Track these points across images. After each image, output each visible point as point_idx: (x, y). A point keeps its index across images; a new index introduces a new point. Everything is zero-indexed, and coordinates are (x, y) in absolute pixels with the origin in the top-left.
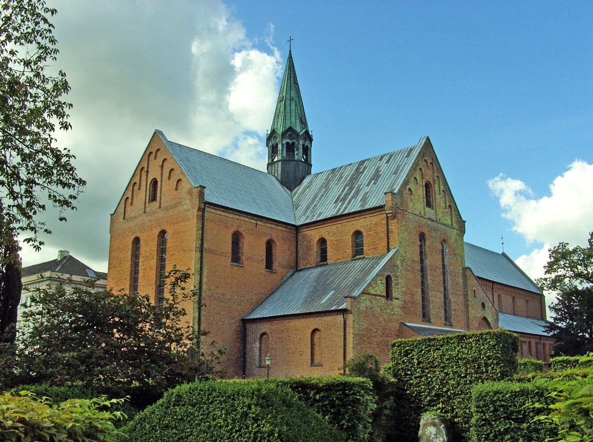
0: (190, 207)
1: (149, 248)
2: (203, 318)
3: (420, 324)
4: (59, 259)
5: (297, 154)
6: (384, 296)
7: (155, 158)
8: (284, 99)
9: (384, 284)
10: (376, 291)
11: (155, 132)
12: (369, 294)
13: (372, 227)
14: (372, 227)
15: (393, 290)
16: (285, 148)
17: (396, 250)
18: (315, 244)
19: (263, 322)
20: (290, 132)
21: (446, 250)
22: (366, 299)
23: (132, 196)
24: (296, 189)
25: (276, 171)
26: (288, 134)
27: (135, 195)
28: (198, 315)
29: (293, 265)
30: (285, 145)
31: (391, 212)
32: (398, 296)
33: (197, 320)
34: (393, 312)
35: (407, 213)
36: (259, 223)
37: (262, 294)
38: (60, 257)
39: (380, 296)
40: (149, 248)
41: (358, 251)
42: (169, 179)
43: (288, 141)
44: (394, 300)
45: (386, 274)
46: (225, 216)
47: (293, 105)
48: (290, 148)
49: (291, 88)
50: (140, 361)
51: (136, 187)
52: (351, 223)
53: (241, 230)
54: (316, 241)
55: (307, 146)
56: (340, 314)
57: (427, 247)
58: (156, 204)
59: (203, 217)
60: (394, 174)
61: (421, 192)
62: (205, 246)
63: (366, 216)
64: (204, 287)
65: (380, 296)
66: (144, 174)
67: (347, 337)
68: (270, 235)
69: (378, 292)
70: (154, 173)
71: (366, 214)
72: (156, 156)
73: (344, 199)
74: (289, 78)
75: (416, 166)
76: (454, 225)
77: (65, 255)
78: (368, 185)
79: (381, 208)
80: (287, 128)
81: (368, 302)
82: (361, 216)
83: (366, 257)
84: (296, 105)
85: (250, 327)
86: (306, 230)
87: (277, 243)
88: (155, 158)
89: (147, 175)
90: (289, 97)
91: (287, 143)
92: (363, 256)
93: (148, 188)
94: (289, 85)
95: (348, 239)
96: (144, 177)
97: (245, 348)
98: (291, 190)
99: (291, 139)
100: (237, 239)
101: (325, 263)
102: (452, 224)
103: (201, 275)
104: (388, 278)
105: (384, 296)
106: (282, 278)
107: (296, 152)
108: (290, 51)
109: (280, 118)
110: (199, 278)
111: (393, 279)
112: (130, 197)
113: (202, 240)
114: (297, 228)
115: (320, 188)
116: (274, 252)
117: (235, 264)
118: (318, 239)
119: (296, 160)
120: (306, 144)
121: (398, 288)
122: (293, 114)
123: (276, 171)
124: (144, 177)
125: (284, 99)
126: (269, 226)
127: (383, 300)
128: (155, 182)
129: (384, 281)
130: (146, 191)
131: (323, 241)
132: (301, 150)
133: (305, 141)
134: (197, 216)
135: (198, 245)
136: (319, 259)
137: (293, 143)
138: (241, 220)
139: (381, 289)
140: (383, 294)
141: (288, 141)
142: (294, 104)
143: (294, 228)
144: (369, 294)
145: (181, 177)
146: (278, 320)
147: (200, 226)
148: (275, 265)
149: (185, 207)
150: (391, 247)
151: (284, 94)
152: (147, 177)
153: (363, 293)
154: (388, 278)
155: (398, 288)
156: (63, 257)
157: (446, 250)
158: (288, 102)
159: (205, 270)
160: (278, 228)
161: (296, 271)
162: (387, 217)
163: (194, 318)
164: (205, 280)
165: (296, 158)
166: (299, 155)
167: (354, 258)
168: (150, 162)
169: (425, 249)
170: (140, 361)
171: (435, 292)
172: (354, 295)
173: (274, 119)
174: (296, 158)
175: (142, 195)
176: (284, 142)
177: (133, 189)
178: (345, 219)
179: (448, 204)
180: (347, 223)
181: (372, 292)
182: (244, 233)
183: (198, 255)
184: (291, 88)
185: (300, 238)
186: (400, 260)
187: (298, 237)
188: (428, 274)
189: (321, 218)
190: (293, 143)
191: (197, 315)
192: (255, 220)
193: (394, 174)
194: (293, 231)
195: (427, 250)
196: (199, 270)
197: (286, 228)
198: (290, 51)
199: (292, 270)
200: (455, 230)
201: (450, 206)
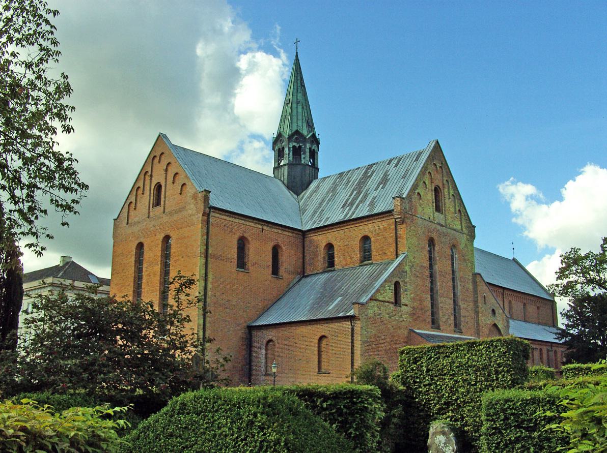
0: (195, 213)
1: (153, 254)
2: (208, 325)
4: (61, 265)
5: (304, 158)
6: (392, 303)
7: (159, 162)
8: (291, 102)
9: (392, 290)
11: (159, 136)
12: (377, 300)
15: (402, 296)
16: (291, 152)
17: (404, 255)
20: (296, 135)
22: (374, 306)
23: (136, 200)
25: (282, 175)
26: (294, 137)
27: (138, 200)
28: (202, 322)
29: (299, 270)
30: (292, 149)
33: (202, 326)
34: (402, 319)
36: (265, 228)
38: (62, 262)
39: (388, 302)
40: (153, 254)
42: (173, 183)
43: (295, 144)
44: (403, 307)
45: (395, 280)
46: (230, 221)
49: (297, 91)
51: (140, 192)
52: (359, 228)
53: (246, 235)
54: (323, 247)
55: (314, 150)
57: (436, 253)
58: (160, 209)
59: (208, 222)
62: (210, 251)
64: (209, 293)
65: (388, 302)
66: (148, 178)
67: (355, 342)
68: (276, 240)
70: (158, 177)
71: (375, 219)
75: (425, 170)
76: (464, 230)
77: (68, 260)
78: (376, 189)
81: (376, 309)
82: (368, 221)
83: (374, 262)
84: (303, 108)
87: (284, 248)
88: (159, 162)
91: (294, 147)
94: (295, 87)
95: (356, 244)
96: (148, 182)
97: (250, 355)
99: (298, 143)
100: (242, 244)
101: (333, 269)
102: (462, 230)
103: (206, 280)
104: (397, 284)
105: (392, 303)
106: (289, 284)
108: (297, 53)
109: (286, 122)
110: (203, 284)
111: (402, 285)
112: (134, 202)
114: (304, 234)
118: (325, 244)
120: (313, 148)
123: (282, 175)
124: (148, 182)
125: (291, 102)
126: (276, 231)
127: (392, 306)
128: (159, 187)
129: (393, 287)
131: (330, 247)
132: (308, 154)
135: (203, 251)
136: (327, 265)
139: (389, 295)
140: (391, 300)
141: (295, 144)
142: (301, 107)
146: (285, 327)
147: (205, 231)
148: (282, 271)
149: (190, 212)
150: (400, 252)
151: (291, 97)
153: (371, 299)
154: (397, 284)
155: (407, 294)
156: (65, 262)
158: (294, 105)
160: (284, 233)
164: (210, 286)
165: (303, 162)
166: (305, 159)
168: (154, 166)
169: (434, 254)
172: (361, 301)
173: (281, 122)
174: (303, 162)
175: (146, 200)
176: (291, 146)
178: (353, 224)
179: (457, 209)
180: (355, 228)
181: (381, 298)
182: (250, 239)
183: (203, 260)
185: (307, 243)
189: (328, 223)
190: (300, 147)
191: (201, 322)
192: (261, 225)
194: (300, 236)
196: (204, 276)
198: (297, 53)
201: (459, 210)
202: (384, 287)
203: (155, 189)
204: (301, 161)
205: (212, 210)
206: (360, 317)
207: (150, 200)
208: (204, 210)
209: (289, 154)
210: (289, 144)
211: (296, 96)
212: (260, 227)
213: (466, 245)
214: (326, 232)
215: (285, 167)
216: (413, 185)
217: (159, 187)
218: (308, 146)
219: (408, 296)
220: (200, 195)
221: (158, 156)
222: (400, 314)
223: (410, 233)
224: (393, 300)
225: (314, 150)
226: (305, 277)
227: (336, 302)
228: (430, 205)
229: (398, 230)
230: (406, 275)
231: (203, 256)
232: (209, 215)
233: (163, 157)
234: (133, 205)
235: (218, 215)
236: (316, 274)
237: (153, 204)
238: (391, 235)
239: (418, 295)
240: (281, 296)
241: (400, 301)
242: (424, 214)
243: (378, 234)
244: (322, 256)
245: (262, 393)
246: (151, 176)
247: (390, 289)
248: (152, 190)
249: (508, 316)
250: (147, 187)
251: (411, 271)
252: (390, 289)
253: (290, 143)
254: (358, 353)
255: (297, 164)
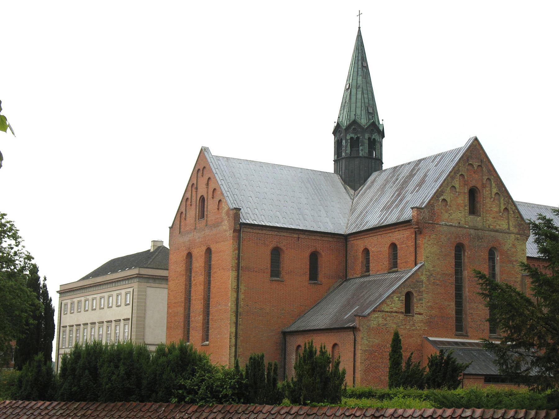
0: (226, 227)
1: (198, 264)
2: (240, 332)
3: (451, 338)
4: (152, 250)
5: (362, 150)
6: (402, 313)
7: (202, 176)
8: (350, 88)
9: (403, 300)
10: (392, 309)
11: (202, 149)
12: (383, 311)
13: (404, 241)
14: (404, 241)
15: (415, 305)
16: (349, 144)
17: (421, 264)
18: (360, 254)
19: (298, 335)
20: (354, 125)
21: (498, 258)
22: (377, 317)
23: (186, 211)
24: (360, 188)
25: (341, 169)
26: (352, 128)
27: (187, 211)
28: (235, 330)
29: (341, 274)
30: (349, 141)
31: (417, 227)
32: (422, 312)
33: (234, 334)
34: (415, 328)
35: (438, 226)
36: (301, 236)
37: (306, 306)
38: (152, 247)
39: (396, 312)
40: (198, 264)
41: (394, 265)
42: (213, 198)
43: (353, 135)
44: (416, 316)
45: (406, 290)
46: (263, 234)
47: (360, 94)
48: (355, 143)
49: (358, 74)
50: (529, 340)
51: (189, 203)
52: (388, 235)
53: (280, 245)
54: (361, 251)
55: (374, 139)
56: (350, 331)
57: (466, 258)
58: (203, 222)
59: (239, 237)
60: (434, 182)
61: (463, 200)
62: (242, 264)
63: (400, 229)
64: (241, 303)
65: (396, 312)
66: (194, 190)
67: (357, 352)
68: (314, 246)
69: (394, 309)
70: (202, 191)
71: (400, 227)
72: (203, 173)
73: (389, 207)
74: (356, 61)
75: (455, 173)
76: (511, 229)
77: (159, 245)
78: (412, 193)
79: (407, 223)
80: (351, 121)
81: (380, 319)
82: (395, 228)
83: (399, 270)
84: (363, 93)
85: (290, 340)
86: (353, 239)
87: (323, 254)
88: (202, 176)
89: (197, 194)
90: (355, 84)
91: (352, 138)
92: (397, 269)
93: (198, 204)
94: (356, 70)
95: (385, 249)
96: (194, 193)
97: (285, 358)
98: (355, 189)
99: (356, 134)
100: (276, 253)
101: (367, 274)
102: (509, 228)
103: (238, 292)
104: (409, 296)
105: (402, 313)
106: (329, 289)
107: (361, 148)
108: (359, 28)
109: (346, 110)
110: (236, 296)
111: (415, 295)
112: (184, 212)
113: (238, 259)
114: (344, 239)
115: (378, 190)
116: (319, 262)
117: (274, 279)
118: (362, 249)
119: (360, 157)
120: (373, 137)
121: (422, 303)
122: (359, 104)
123: (341, 169)
124: (194, 193)
125: (350, 88)
126: (313, 238)
127: (401, 316)
128: (203, 199)
129: (403, 298)
130: (196, 208)
131: (366, 251)
132: (367, 145)
133: (372, 134)
134: (233, 236)
135: (234, 265)
136: (365, 269)
137: (358, 138)
138: (281, 236)
139: (398, 304)
140: (401, 311)
141: (353, 135)
142: (361, 92)
143: (342, 237)
144: (383, 311)
145: (221, 197)
146: (309, 334)
147: (237, 246)
148: (321, 276)
149: (224, 227)
150: (418, 261)
151: (351, 81)
152: (197, 194)
153: (374, 311)
154: (409, 296)
155: (422, 303)
156: (156, 248)
157: (498, 258)
158: (354, 91)
159: (242, 287)
160: (324, 239)
161: (345, 281)
162: (415, 231)
163: (231, 333)
164: (242, 296)
165: (361, 155)
166: (363, 151)
167: (391, 271)
168: (199, 178)
169: (464, 259)
170: (529, 340)
171: (476, 304)
172: (364, 314)
173: (341, 110)
174: (361, 155)
175: (192, 213)
176: (348, 137)
177: (186, 204)
178: (383, 231)
179: (503, 207)
180: (385, 235)
181: (387, 309)
182: (284, 248)
183: (234, 274)
184: (358, 74)
185: (349, 247)
186: (426, 275)
187: (348, 246)
188: (467, 285)
189: (365, 228)
190: (358, 138)
191: (233, 330)
192: (297, 234)
193: (434, 182)
194: (341, 240)
195: (466, 260)
196: (236, 287)
197: (333, 238)
198: (359, 28)
199: (340, 280)
200: (513, 235)
201: (506, 209)
202: (392, 298)
203: (200, 202)
204: (359, 153)
205: (242, 226)
206: (361, 328)
207: (120, 278)
208: (234, 227)
209: (346, 146)
210: (346, 136)
211: (356, 80)
212: (295, 236)
213: (513, 245)
214: (363, 237)
215: (343, 160)
216: (435, 193)
217: (203, 199)
218: (367, 136)
219: (424, 305)
220: (231, 213)
221: (201, 170)
222: (411, 323)
223: (430, 243)
224: (403, 310)
225: (374, 139)
226: (347, 280)
227: (348, 316)
228: (461, 208)
229: (417, 240)
230: (422, 285)
231: (234, 269)
232: (240, 230)
233: (205, 170)
234: (184, 216)
235: (250, 230)
236: (357, 278)
237: (199, 216)
238: (411, 243)
239: (437, 303)
240: (320, 301)
241: (413, 310)
242: (451, 219)
243: (402, 242)
244: (360, 260)
245: (320, 391)
246: (197, 188)
247: (399, 300)
248: (198, 202)
249: (241, 368)
250: (194, 198)
251: (428, 280)
252: (399, 300)
253: (348, 135)
254: (358, 360)
255: (354, 157)
